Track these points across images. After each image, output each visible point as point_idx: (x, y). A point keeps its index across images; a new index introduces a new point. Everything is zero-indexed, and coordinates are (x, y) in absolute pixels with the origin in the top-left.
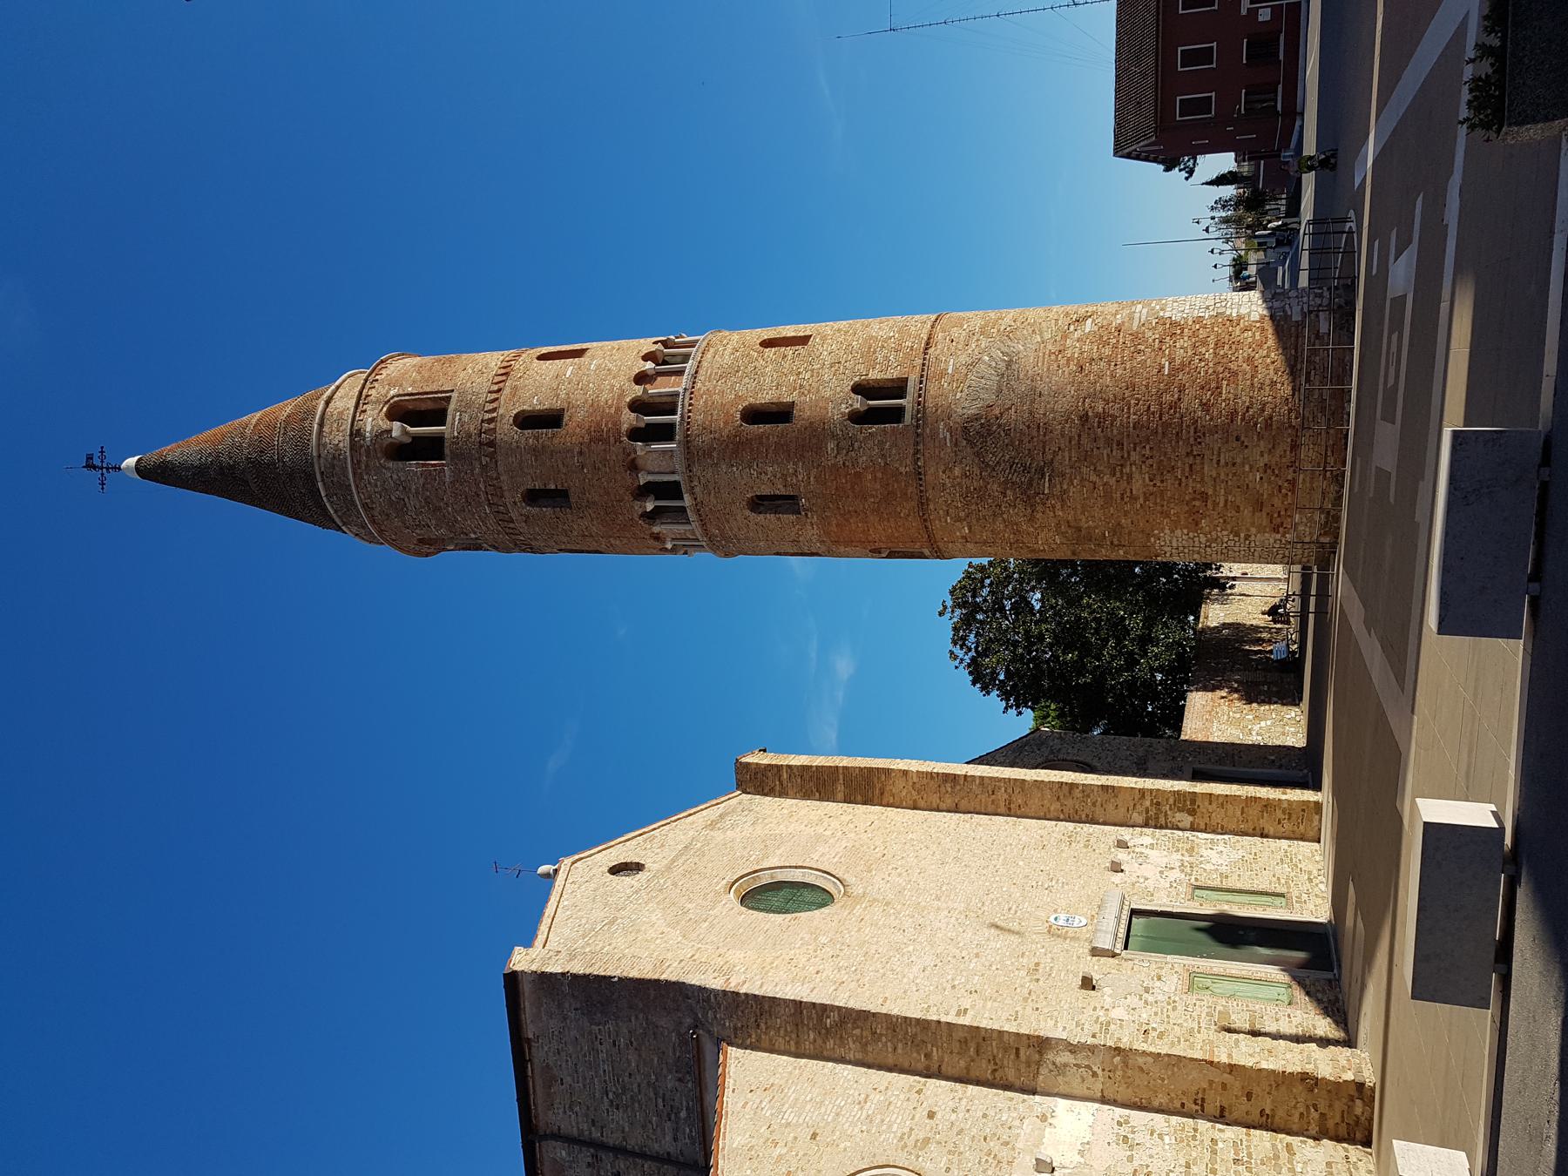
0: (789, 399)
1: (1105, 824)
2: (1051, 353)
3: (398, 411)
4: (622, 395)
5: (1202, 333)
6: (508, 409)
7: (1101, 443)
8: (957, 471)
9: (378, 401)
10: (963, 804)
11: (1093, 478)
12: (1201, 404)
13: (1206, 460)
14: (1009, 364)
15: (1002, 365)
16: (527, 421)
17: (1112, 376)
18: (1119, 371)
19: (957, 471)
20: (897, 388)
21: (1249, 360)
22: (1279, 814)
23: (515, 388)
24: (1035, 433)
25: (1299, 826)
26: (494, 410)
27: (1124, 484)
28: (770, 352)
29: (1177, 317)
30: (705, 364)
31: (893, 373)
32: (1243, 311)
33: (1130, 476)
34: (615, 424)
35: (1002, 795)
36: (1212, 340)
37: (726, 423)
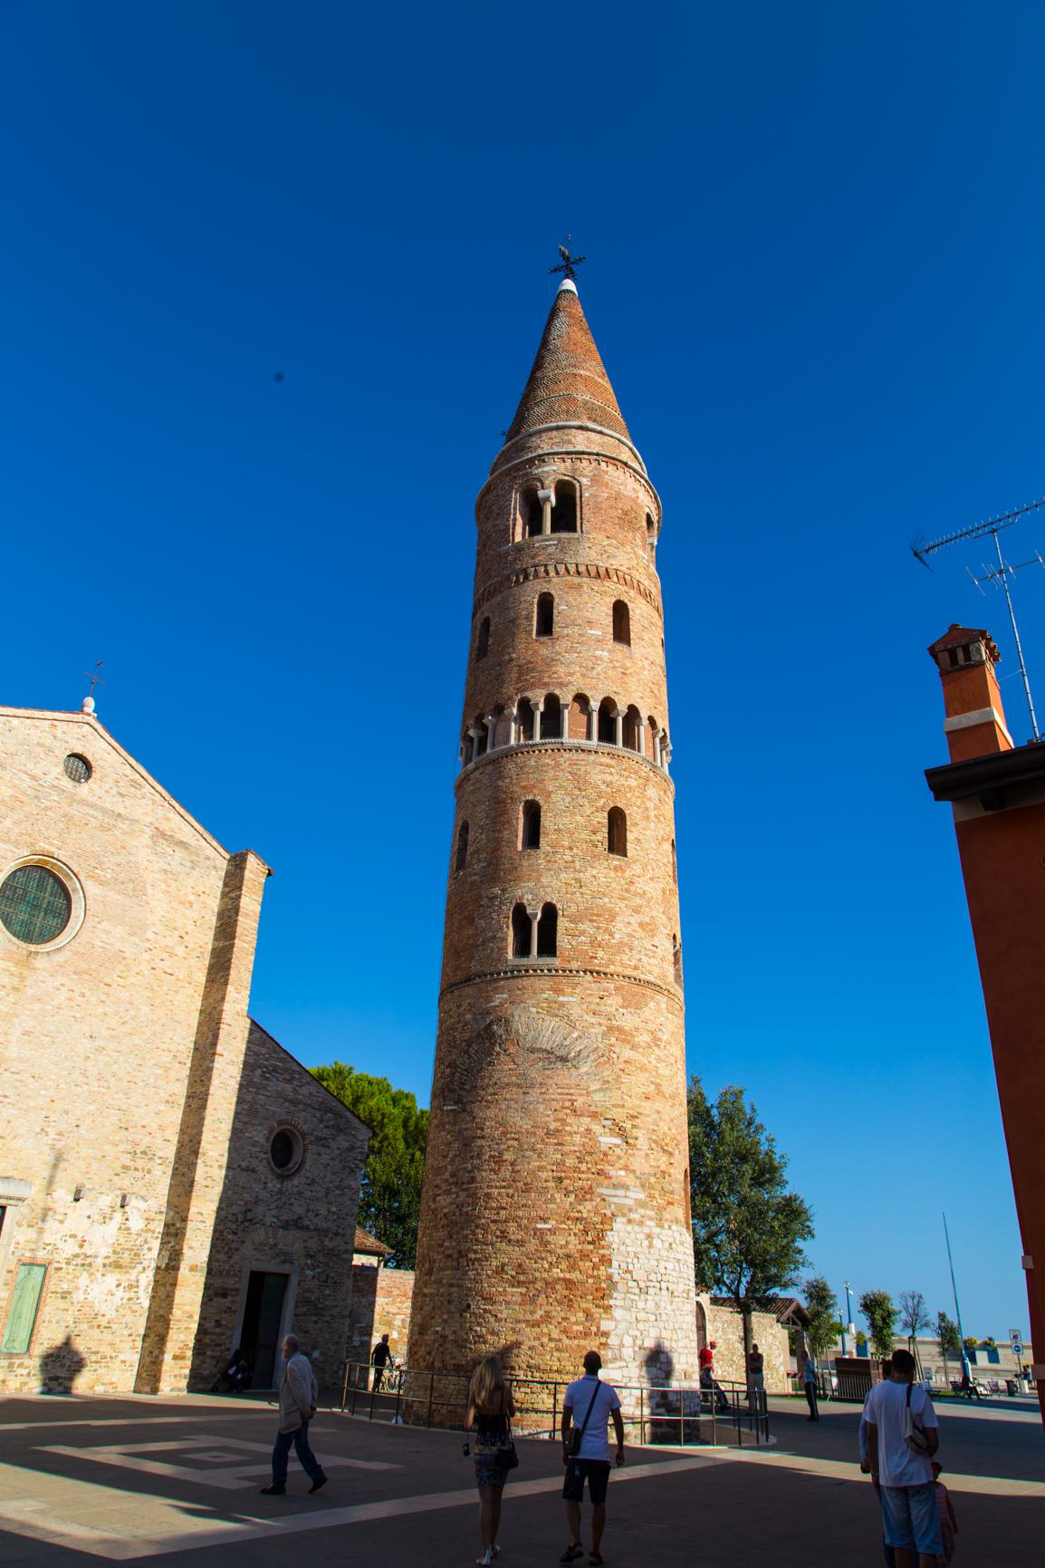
0: (542, 842)
2: (573, 1101)
3: (566, 492)
4: (561, 685)
6: (555, 586)
9: (574, 470)
12: (503, 1265)
14: (564, 1059)
15: (562, 1053)
16: (546, 603)
17: (540, 1168)
18: (544, 1175)
19: (469, 1017)
20: (548, 947)
21: (547, 1317)
25: (150, 1372)
28: (603, 818)
29: (610, 1236)
30: (592, 757)
31: (562, 941)
32: (617, 1313)
33: (448, 1193)
37: (524, 788)
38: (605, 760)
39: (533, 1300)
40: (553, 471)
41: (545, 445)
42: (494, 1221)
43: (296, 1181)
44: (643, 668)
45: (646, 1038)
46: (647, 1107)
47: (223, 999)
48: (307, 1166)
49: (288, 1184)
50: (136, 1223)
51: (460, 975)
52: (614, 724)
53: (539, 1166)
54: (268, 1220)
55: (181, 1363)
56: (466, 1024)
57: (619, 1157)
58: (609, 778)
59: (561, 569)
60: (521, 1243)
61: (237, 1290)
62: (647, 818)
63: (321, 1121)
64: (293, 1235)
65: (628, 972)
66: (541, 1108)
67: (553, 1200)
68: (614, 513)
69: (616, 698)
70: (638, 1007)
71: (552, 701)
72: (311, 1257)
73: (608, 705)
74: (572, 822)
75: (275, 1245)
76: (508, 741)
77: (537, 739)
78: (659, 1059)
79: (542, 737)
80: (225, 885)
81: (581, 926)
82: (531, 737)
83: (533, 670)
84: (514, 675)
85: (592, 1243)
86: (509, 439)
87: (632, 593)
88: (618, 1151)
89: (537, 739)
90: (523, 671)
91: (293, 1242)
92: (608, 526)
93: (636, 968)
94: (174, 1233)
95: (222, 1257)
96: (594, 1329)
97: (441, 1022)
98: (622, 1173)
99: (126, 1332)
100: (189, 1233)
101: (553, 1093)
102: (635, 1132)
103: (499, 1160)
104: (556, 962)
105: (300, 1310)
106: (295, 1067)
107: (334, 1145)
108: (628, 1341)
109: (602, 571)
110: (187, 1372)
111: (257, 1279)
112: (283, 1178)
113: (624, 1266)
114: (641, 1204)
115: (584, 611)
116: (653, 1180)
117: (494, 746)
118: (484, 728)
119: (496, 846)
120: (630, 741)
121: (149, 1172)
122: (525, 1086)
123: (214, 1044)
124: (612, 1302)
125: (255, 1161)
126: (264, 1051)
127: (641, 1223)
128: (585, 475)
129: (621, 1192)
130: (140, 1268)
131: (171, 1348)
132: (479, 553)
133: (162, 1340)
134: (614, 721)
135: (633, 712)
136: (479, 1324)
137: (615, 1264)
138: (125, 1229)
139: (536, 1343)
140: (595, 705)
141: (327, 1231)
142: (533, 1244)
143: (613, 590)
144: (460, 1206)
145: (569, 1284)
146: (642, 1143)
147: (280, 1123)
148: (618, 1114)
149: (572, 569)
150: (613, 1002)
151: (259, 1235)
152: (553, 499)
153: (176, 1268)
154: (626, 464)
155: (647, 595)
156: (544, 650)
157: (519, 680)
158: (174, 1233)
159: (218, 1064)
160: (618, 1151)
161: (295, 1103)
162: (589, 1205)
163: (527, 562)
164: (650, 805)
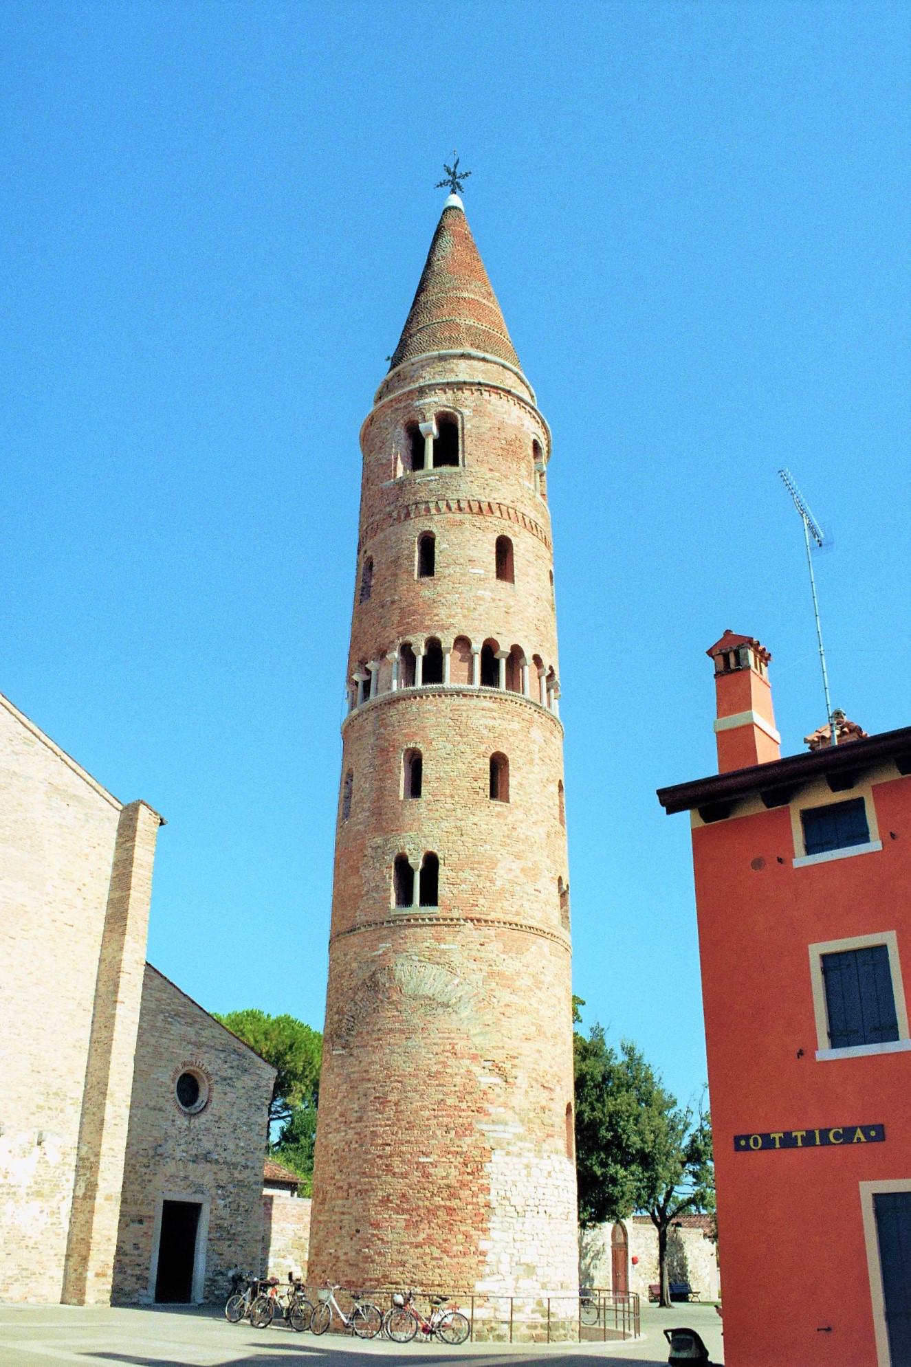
1: (81, 1124)
2: (453, 1046)
3: (449, 427)
4: (443, 628)
5: (465, 1194)
6: (435, 525)
7: (363, 1102)
8: (355, 965)
9: (456, 400)
10: (100, 1001)
11: (340, 1096)
13: (345, 1202)
14: (446, 1005)
16: (427, 544)
17: (423, 1108)
18: (426, 1114)
19: (355, 965)
20: (430, 897)
22: (80, 1270)
23: (462, 523)
24: (374, 1036)
26: (438, 510)
27: (334, 1125)
28: (485, 765)
29: (488, 1168)
30: (475, 701)
31: (443, 890)
33: (338, 1131)
34: (414, 628)
35: (104, 1033)
36: (454, 1203)
37: (406, 735)
38: (487, 704)
39: (416, 1225)
40: (437, 402)
41: (427, 377)
42: (380, 1157)
43: (203, 1118)
46: (527, 1047)
47: (121, 949)
48: (213, 1105)
50: (54, 1157)
52: (496, 666)
53: (420, 1106)
54: (178, 1154)
55: (103, 1279)
57: (499, 1096)
58: (490, 722)
59: (442, 505)
60: (404, 1175)
62: (531, 762)
64: (202, 1167)
65: (509, 918)
66: (423, 1051)
67: (434, 1136)
68: (497, 444)
69: (495, 637)
70: (520, 952)
71: (434, 648)
72: (219, 1187)
73: (489, 649)
74: (453, 769)
75: (186, 1178)
76: (389, 688)
77: (419, 684)
79: (425, 681)
80: (120, 835)
81: (462, 875)
82: (411, 680)
83: (415, 612)
84: (396, 619)
85: (472, 1173)
86: (393, 366)
87: (516, 527)
88: (497, 1090)
89: (419, 684)
90: (403, 613)
92: (492, 458)
93: (518, 914)
94: (87, 1166)
95: (136, 1187)
96: (473, 1249)
97: (331, 970)
98: (502, 1110)
99: (52, 1253)
100: (102, 1167)
101: (435, 1037)
102: (514, 1072)
103: (383, 1100)
107: (239, 1084)
108: (505, 1258)
109: (485, 507)
110: (110, 1287)
111: (172, 1209)
113: (502, 1193)
114: (521, 1138)
115: (466, 548)
116: (532, 1115)
117: (377, 693)
118: (368, 672)
119: (381, 793)
120: (514, 682)
121: (62, 1111)
122: (407, 1032)
123: (116, 992)
124: (490, 1225)
125: (162, 1101)
126: (164, 996)
128: (467, 408)
129: (500, 1128)
130: (59, 1197)
131: (93, 1266)
132: (363, 486)
133: (85, 1259)
134: (497, 662)
135: (516, 654)
136: (368, 1247)
137: (493, 1192)
138: (44, 1162)
139: (419, 1262)
140: (477, 646)
141: (235, 1165)
142: (415, 1176)
144: (349, 1143)
145: (450, 1211)
146: (522, 1082)
147: (184, 1064)
148: (498, 1056)
149: (454, 505)
151: (171, 1168)
152: (435, 430)
153: (93, 1198)
155: (533, 527)
156: (426, 590)
157: (400, 624)
158: (87, 1166)
159: (120, 1010)
161: (198, 1045)
162: (468, 1140)
163: (409, 499)
164: (535, 748)
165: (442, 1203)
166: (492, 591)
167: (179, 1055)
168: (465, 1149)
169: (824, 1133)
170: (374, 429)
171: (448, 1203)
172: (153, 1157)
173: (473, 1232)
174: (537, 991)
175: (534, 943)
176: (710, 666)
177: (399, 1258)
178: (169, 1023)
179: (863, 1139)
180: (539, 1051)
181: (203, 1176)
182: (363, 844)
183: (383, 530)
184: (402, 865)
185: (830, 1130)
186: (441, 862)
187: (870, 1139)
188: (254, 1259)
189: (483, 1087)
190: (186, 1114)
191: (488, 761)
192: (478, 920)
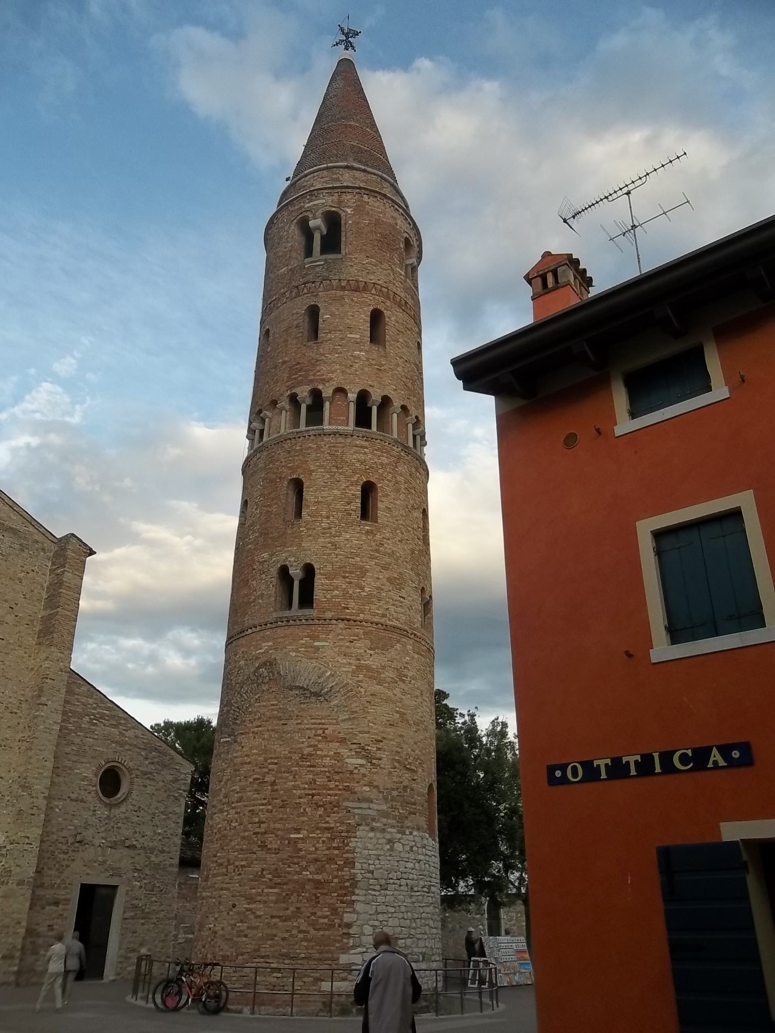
3: (333, 221)
4: (323, 381)
7: (243, 784)
17: (296, 787)
20: (307, 600)
27: (219, 806)
28: (357, 491)
31: (319, 594)
32: (358, 907)
39: (285, 900)
44: (398, 365)
45: (392, 674)
49: (116, 812)
51: (238, 628)
54: (97, 842)
56: (240, 668)
57: (364, 775)
61: (69, 900)
62: (398, 490)
63: (146, 759)
69: (370, 390)
70: (385, 648)
71: (317, 397)
72: (137, 870)
73: (363, 397)
75: (104, 862)
77: (303, 427)
78: (404, 693)
79: (307, 425)
82: (296, 424)
89: (303, 427)
91: (122, 859)
93: (384, 616)
98: (367, 789)
104: (314, 613)
105: (127, 915)
106: (122, 715)
107: (158, 777)
108: (368, 930)
111: (88, 891)
112: (110, 806)
114: (386, 815)
120: (383, 425)
127: (383, 831)
134: (370, 410)
136: (242, 922)
140: (352, 396)
141: (152, 851)
143: (371, 301)
145: (318, 884)
146: (385, 762)
148: (363, 739)
150: (361, 646)
151: (89, 853)
154: (385, 196)
160: (363, 770)
161: (121, 744)
165: (310, 877)
166: (366, 351)
167: (102, 752)
168: (332, 825)
169: (666, 757)
170: (274, 230)
171: (316, 877)
172: (72, 844)
173: (339, 905)
174: (400, 683)
175: (398, 641)
176: (528, 291)
177: (269, 931)
178: (95, 724)
179: (722, 763)
180: (402, 736)
181: (120, 861)
182: (253, 561)
183: (278, 308)
184: (284, 572)
185: (674, 752)
186: (317, 571)
187: (732, 764)
188: (166, 935)
189: (351, 768)
190: (106, 805)
191: (359, 488)
192: (348, 620)
